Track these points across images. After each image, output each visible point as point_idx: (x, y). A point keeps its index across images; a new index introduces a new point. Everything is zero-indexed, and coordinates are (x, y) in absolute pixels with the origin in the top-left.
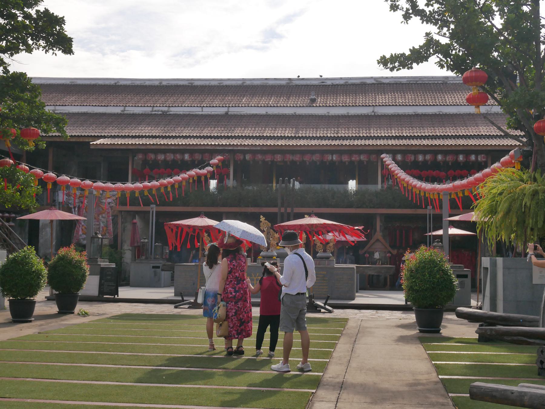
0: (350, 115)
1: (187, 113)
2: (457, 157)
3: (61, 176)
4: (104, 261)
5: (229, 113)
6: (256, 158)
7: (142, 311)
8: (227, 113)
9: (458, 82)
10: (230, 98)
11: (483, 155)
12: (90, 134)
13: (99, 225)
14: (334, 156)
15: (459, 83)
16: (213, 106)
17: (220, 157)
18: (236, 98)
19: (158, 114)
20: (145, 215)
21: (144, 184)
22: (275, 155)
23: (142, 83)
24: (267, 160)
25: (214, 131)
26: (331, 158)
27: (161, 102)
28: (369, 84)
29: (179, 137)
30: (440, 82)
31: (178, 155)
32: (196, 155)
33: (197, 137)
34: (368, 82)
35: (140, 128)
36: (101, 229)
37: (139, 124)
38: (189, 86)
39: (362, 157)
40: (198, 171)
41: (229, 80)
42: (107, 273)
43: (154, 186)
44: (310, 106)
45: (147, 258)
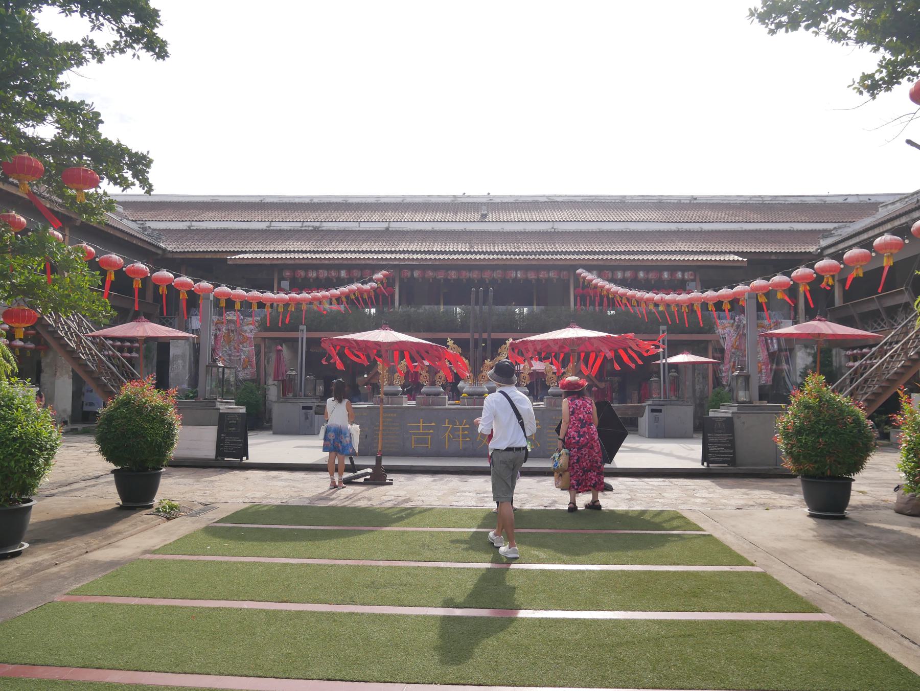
0: (527, 231)
1: (342, 229)
2: (661, 275)
3: (159, 271)
4: (227, 402)
5: (390, 229)
6: (426, 276)
7: (283, 495)
8: (387, 229)
9: (636, 201)
10: (389, 214)
11: (690, 273)
12: (228, 250)
13: (240, 355)
14: (519, 272)
15: (638, 203)
16: (372, 221)
17: (384, 272)
18: (396, 214)
19: (308, 230)
20: (292, 343)
21: (290, 295)
22: (449, 272)
23: (291, 200)
24: (440, 277)
25: (375, 246)
26: (515, 275)
27: (312, 217)
28: (541, 202)
29: (334, 252)
30: (617, 201)
31: (332, 272)
32: (354, 271)
33: (354, 252)
34: (541, 200)
35: (287, 243)
36: (242, 361)
37: (288, 239)
38: (343, 203)
40: (360, 285)
41: (387, 197)
42: (230, 422)
43: (305, 300)
44: (482, 221)
45: (295, 396)
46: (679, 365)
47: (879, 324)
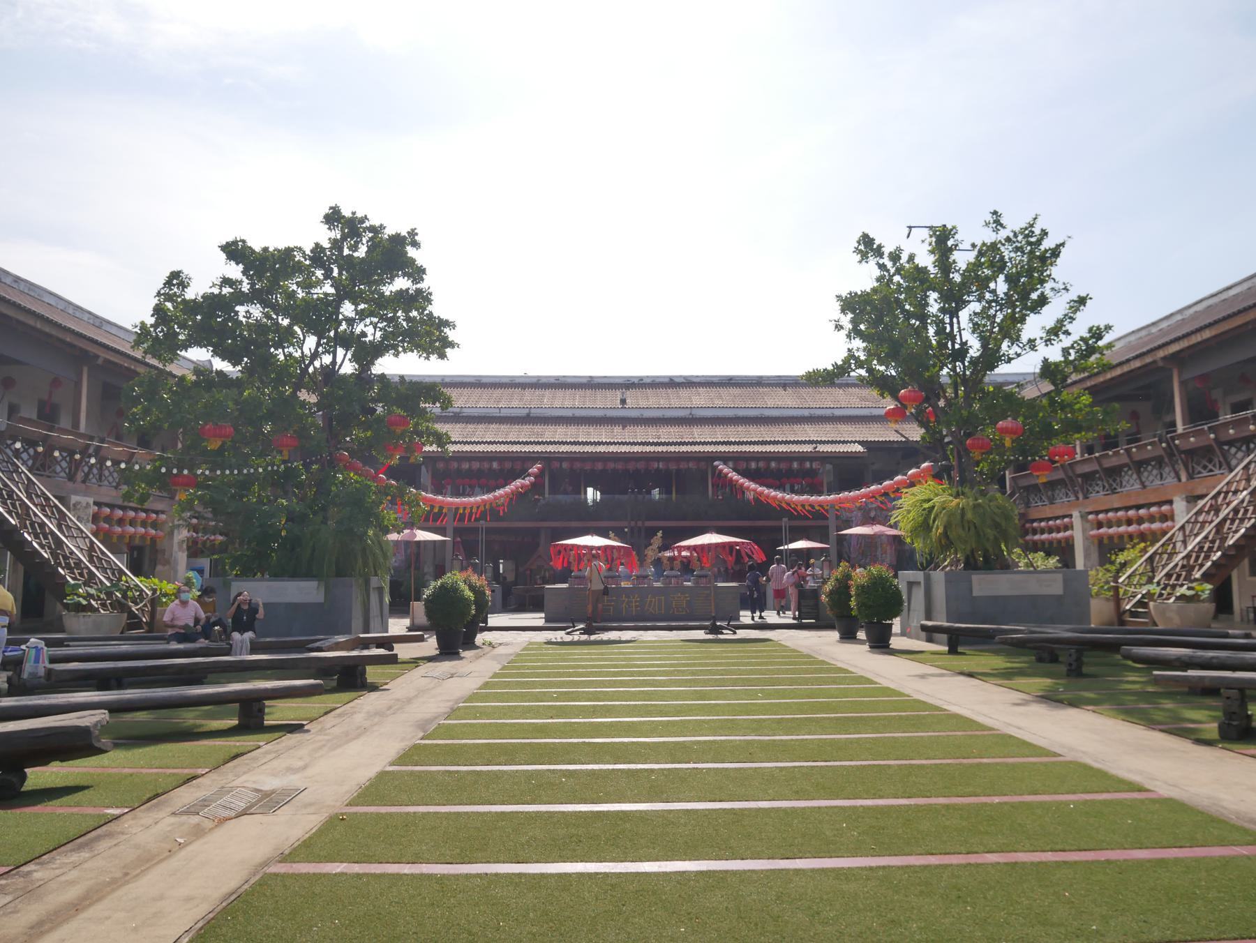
5: (531, 415)
8: (528, 415)
14: (661, 463)
39: (691, 465)
46: (925, 639)
47: (1205, 467)
